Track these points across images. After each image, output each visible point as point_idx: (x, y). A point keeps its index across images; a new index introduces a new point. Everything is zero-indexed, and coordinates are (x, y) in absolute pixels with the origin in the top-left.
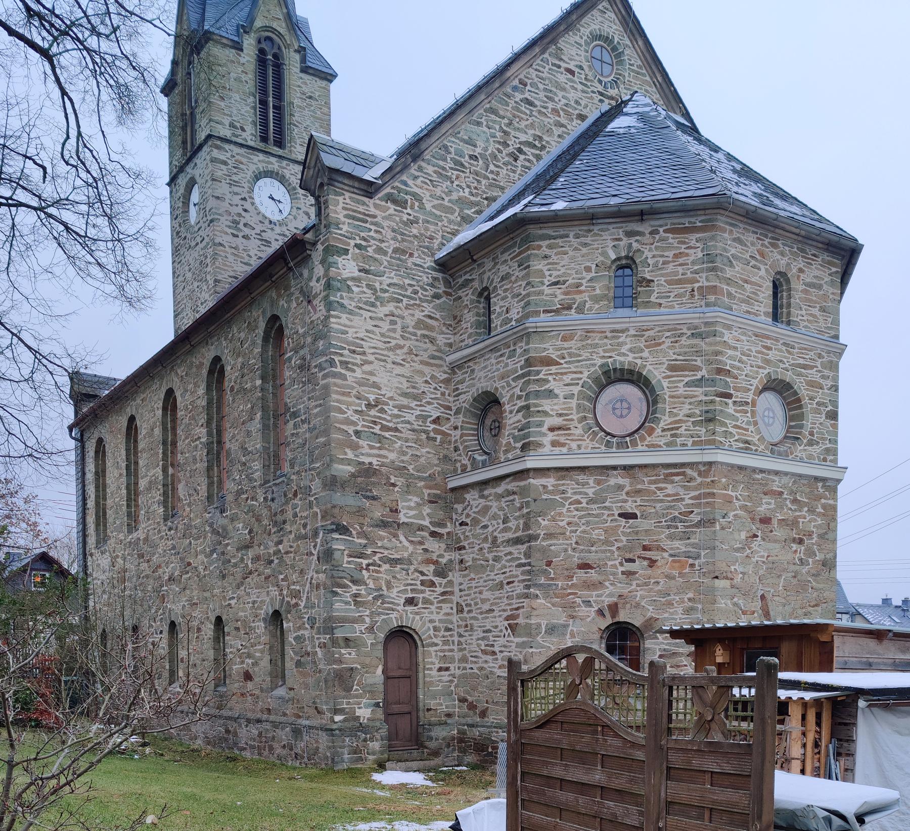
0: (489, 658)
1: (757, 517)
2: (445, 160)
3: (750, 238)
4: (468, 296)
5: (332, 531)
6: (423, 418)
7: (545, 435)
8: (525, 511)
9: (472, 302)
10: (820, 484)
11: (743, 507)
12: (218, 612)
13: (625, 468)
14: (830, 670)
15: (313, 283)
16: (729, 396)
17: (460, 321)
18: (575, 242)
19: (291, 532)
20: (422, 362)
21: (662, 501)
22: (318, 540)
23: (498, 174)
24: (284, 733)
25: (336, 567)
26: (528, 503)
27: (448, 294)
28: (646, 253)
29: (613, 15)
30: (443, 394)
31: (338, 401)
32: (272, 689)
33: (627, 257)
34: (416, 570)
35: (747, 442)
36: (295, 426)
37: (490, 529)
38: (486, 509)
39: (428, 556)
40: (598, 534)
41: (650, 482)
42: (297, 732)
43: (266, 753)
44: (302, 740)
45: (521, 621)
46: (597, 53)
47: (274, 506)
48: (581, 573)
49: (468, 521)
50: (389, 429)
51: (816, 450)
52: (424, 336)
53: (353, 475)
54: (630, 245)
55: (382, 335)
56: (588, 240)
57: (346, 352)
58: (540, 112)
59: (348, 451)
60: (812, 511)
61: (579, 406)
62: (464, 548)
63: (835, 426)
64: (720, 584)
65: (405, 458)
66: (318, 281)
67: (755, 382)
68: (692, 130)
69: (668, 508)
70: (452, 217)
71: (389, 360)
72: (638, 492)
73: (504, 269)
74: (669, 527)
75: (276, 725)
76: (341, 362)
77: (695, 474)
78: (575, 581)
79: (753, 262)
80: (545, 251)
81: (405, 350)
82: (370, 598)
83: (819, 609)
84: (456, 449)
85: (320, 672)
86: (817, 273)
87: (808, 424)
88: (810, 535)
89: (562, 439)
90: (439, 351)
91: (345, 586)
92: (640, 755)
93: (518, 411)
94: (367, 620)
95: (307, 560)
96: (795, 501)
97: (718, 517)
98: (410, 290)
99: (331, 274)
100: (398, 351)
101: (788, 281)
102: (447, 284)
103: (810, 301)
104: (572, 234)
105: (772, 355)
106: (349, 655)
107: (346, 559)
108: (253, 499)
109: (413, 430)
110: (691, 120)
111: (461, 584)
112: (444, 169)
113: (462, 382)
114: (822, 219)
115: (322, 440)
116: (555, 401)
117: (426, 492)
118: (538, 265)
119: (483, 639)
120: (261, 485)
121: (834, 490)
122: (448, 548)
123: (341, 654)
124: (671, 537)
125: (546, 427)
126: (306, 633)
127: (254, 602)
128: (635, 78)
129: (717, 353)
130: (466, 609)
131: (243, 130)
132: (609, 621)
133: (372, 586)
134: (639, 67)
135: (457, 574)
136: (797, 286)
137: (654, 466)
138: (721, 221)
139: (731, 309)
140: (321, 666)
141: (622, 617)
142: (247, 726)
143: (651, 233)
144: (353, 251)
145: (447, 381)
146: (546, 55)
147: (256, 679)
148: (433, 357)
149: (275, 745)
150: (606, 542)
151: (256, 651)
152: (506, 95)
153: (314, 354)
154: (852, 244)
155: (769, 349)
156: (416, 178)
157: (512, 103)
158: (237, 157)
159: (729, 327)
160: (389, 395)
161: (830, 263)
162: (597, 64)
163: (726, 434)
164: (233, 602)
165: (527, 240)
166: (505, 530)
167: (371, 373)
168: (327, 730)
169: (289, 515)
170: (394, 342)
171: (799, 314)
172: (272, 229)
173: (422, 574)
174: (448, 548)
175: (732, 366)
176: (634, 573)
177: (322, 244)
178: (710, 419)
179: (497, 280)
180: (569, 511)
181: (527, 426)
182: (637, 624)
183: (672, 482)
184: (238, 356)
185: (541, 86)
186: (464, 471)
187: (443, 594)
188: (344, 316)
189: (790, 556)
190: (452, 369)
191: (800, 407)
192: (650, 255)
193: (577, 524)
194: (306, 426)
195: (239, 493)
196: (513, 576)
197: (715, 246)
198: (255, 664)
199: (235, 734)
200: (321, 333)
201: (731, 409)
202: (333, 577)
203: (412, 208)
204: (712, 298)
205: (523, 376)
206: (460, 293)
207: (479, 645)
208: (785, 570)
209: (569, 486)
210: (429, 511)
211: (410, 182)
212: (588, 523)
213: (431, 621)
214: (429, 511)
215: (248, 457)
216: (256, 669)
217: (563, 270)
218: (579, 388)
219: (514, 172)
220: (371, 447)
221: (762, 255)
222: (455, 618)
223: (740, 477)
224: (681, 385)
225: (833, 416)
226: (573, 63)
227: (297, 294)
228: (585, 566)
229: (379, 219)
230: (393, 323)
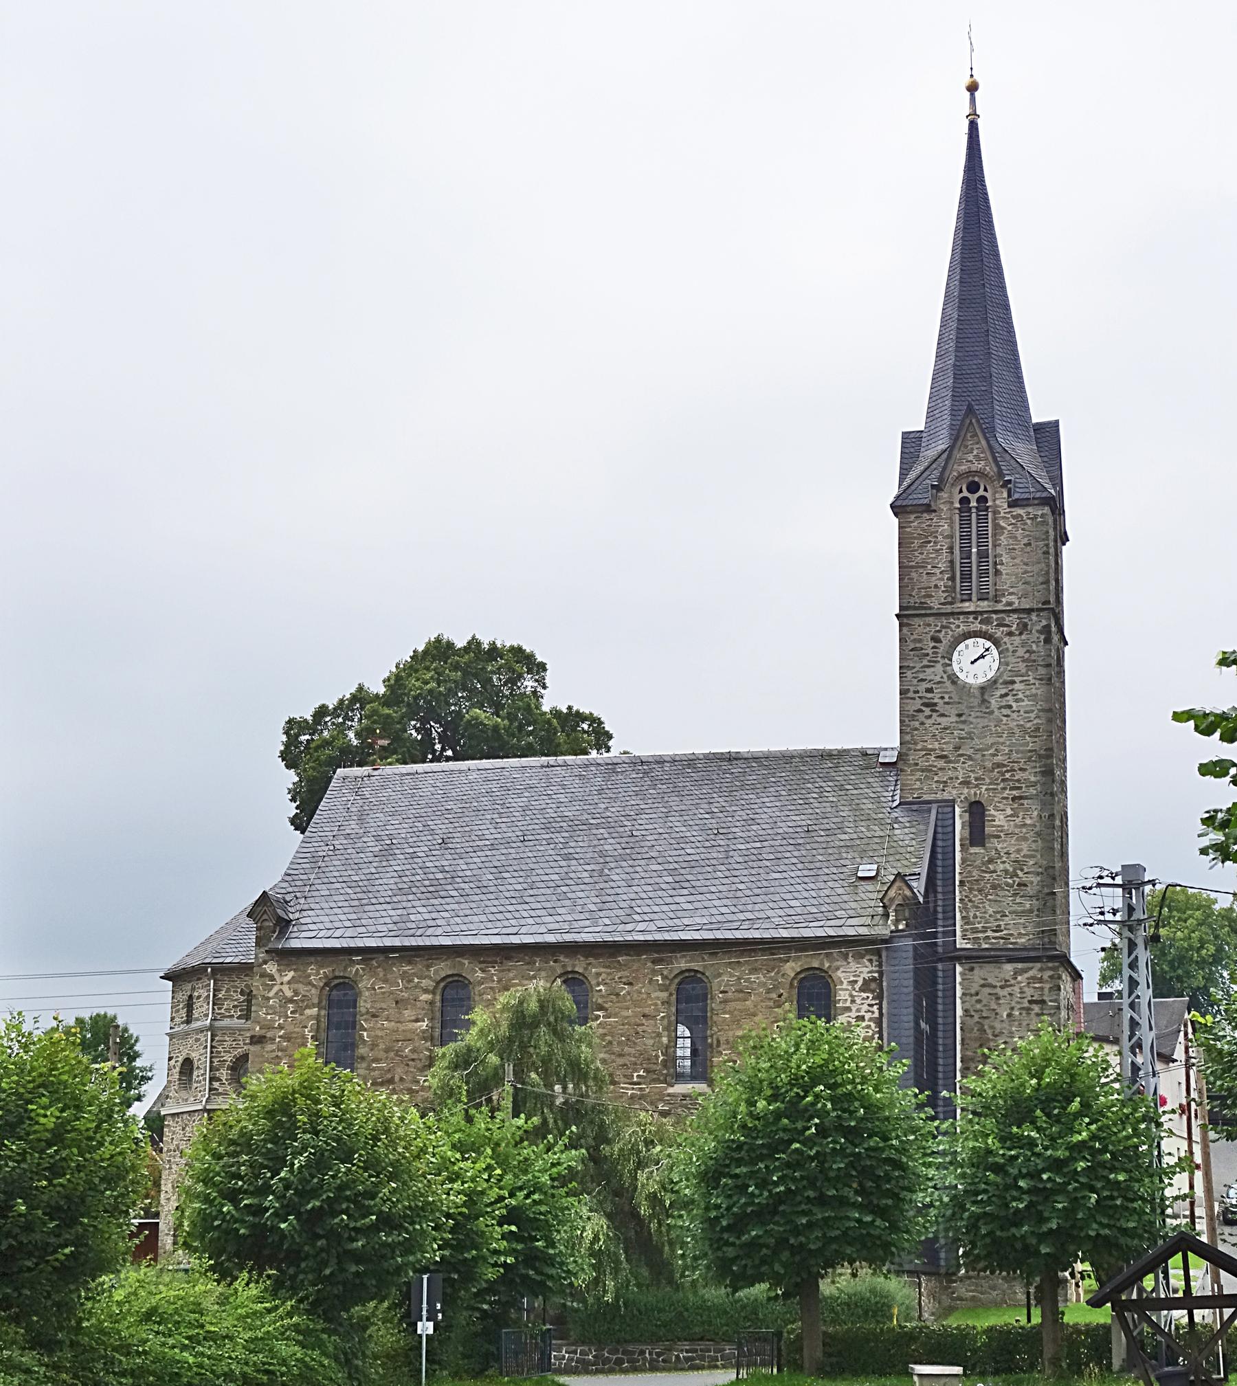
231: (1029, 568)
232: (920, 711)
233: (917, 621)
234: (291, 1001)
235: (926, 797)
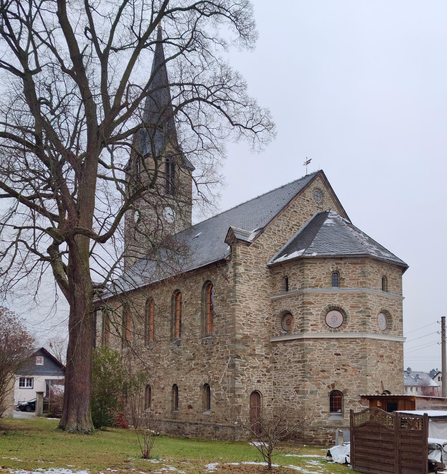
0: (287, 402)
1: (379, 355)
2: (270, 232)
3: (375, 266)
4: (279, 277)
5: (235, 358)
6: (263, 318)
7: (309, 327)
8: (302, 352)
9: (280, 280)
10: (398, 343)
11: (375, 352)
12: (175, 383)
13: (336, 339)
14: (415, 410)
15: (228, 273)
16: (370, 316)
17: (275, 285)
18: (319, 265)
19: (215, 356)
20: (263, 299)
21: (349, 350)
22: (229, 360)
23: (286, 235)
24: (210, 428)
25: (236, 370)
26: (303, 350)
27: (271, 276)
28: (343, 270)
29: (321, 181)
30: (269, 310)
31: (238, 314)
32: (203, 412)
33: (336, 271)
34: (261, 370)
35: (376, 331)
36: (218, 320)
37: (288, 357)
38: (286, 350)
39: (264, 365)
40: (327, 360)
41: (345, 344)
42: (216, 428)
43: (200, 435)
44: (219, 431)
45: (300, 389)
46: (316, 194)
47: (206, 346)
48: (322, 373)
49: (278, 353)
50: (253, 322)
51: (396, 332)
52: (264, 290)
53: (242, 338)
54: (337, 267)
55: (251, 291)
56: (323, 265)
57: (240, 297)
58: (299, 214)
59: (240, 330)
60: (396, 352)
61: (321, 318)
62: (277, 363)
63: (402, 324)
64: (369, 378)
65: (257, 332)
66: (230, 273)
67: (378, 311)
68: (350, 224)
69: (352, 352)
70: (272, 250)
71: (253, 299)
72: (341, 347)
73: (293, 271)
74: (351, 359)
75: (205, 425)
76: (239, 301)
77: (360, 342)
78: (320, 376)
79: (376, 273)
80: (309, 267)
81: (258, 295)
82: (246, 380)
83: (399, 385)
84: (273, 328)
85: (228, 406)
86: (395, 275)
87: (394, 324)
88: (395, 360)
89: (315, 329)
90: (268, 295)
91: (239, 377)
92: (393, 433)
93: (299, 318)
94: (245, 388)
95: (223, 367)
96: (390, 349)
97: (367, 355)
98: (260, 275)
99: (237, 272)
100: (256, 296)
101: (386, 278)
102: (271, 272)
103: (393, 284)
104: (318, 263)
105: (382, 302)
106: (239, 400)
107: (239, 367)
108: (195, 343)
109: (260, 322)
110: (350, 222)
111: (275, 375)
112: (270, 235)
113: (276, 306)
114: (396, 258)
115: (232, 326)
116: (313, 316)
117: (264, 343)
118: (307, 272)
119: (284, 395)
120: (200, 338)
121: (402, 345)
122: (270, 363)
123: (237, 400)
124: (352, 362)
125: (310, 324)
126: (222, 393)
127: (195, 380)
128: (328, 201)
129: (366, 303)
130: (277, 384)
132: (331, 390)
133: (247, 376)
134: (329, 197)
135: (273, 372)
136: (389, 280)
137: (346, 338)
138: (367, 261)
139: (370, 288)
140: (229, 404)
141: (336, 388)
142: (190, 426)
143: (344, 264)
144: (243, 264)
145: (270, 305)
146: (301, 196)
147: (195, 408)
148: (266, 297)
149: (205, 432)
150: (330, 363)
151: (195, 398)
152: (288, 210)
153: (229, 297)
154: (405, 266)
155: (381, 300)
156: (262, 239)
157: (290, 212)
159: (370, 294)
160: (253, 311)
161: (398, 271)
162: (316, 197)
163: (370, 328)
164: (183, 379)
165: (303, 263)
166: (294, 358)
167: (248, 304)
168: (231, 427)
169: (215, 350)
170: (255, 293)
171: (390, 288)
173: (262, 371)
174: (270, 363)
175: (371, 306)
176: (340, 374)
177: (233, 261)
178: (364, 324)
179: (290, 274)
180: (317, 352)
181: (303, 324)
182: (341, 391)
183: (352, 344)
184: (189, 291)
185: (299, 206)
186: (277, 335)
187: (269, 378)
188: (240, 285)
189: (389, 368)
190: (272, 301)
191: (391, 318)
192: (344, 271)
193: (320, 357)
194: (224, 321)
195: (188, 340)
196: (297, 374)
197: (365, 269)
198: (195, 402)
199: (183, 429)
200: (232, 290)
201: (370, 321)
202: (235, 373)
203: (260, 248)
204: (364, 285)
205: (301, 307)
206: (275, 276)
207: (282, 397)
208: (388, 372)
209: (318, 344)
210: (264, 350)
211: (260, 240)
212: (324, 357)
213: (265, 388)
214: (264, 350)
215: (193, 328)
216: (195, 405)
217: (315, 274)
218: (321, 312)
219: (291, 234)
220: (247, 329)
221: (379, 271)
222: (272, 387)
223: (373, 342)
224: (355, 312)
225: (401, 320)
226: (309, 198)
227: (220, 275)
228: (323, 371)
229: (251, 253)
230: (254, 287)
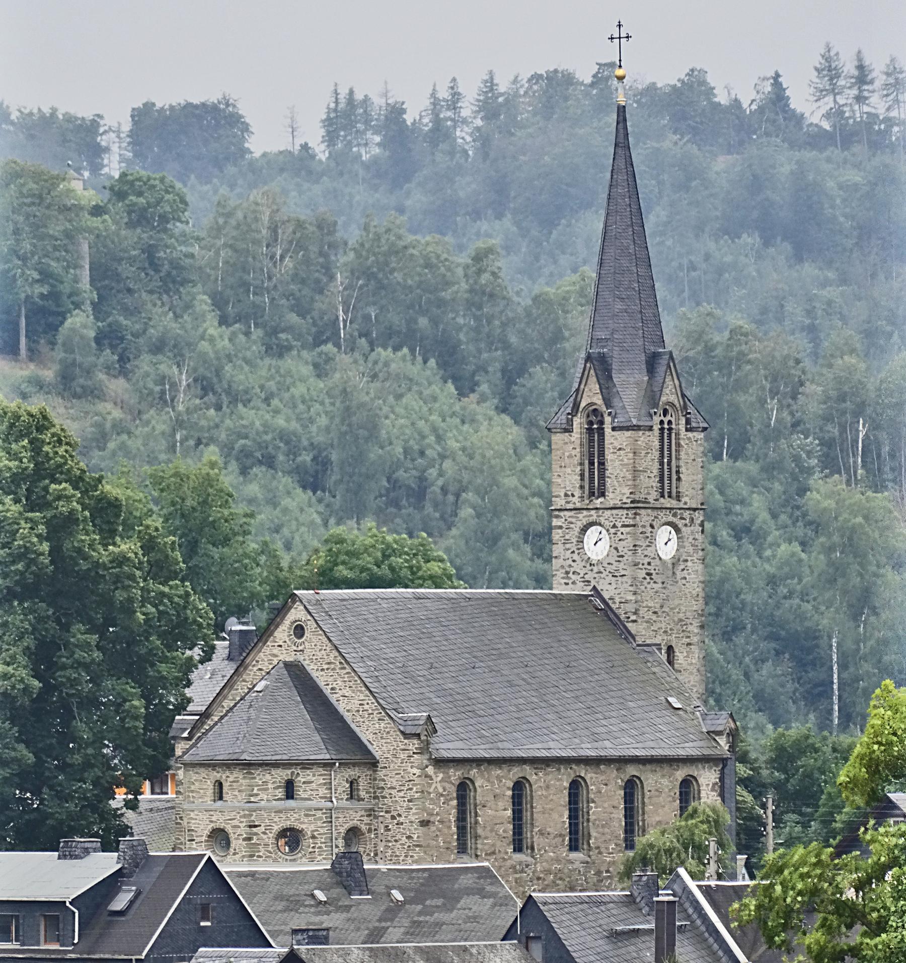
16: (193, 840)
131: (573, 495)
158: (569, 520)
172: (592, 570)
231: (695, 478)
232: (645, 578)
233: (642, 512)
234: (442, 795)
235: (648, 642)
